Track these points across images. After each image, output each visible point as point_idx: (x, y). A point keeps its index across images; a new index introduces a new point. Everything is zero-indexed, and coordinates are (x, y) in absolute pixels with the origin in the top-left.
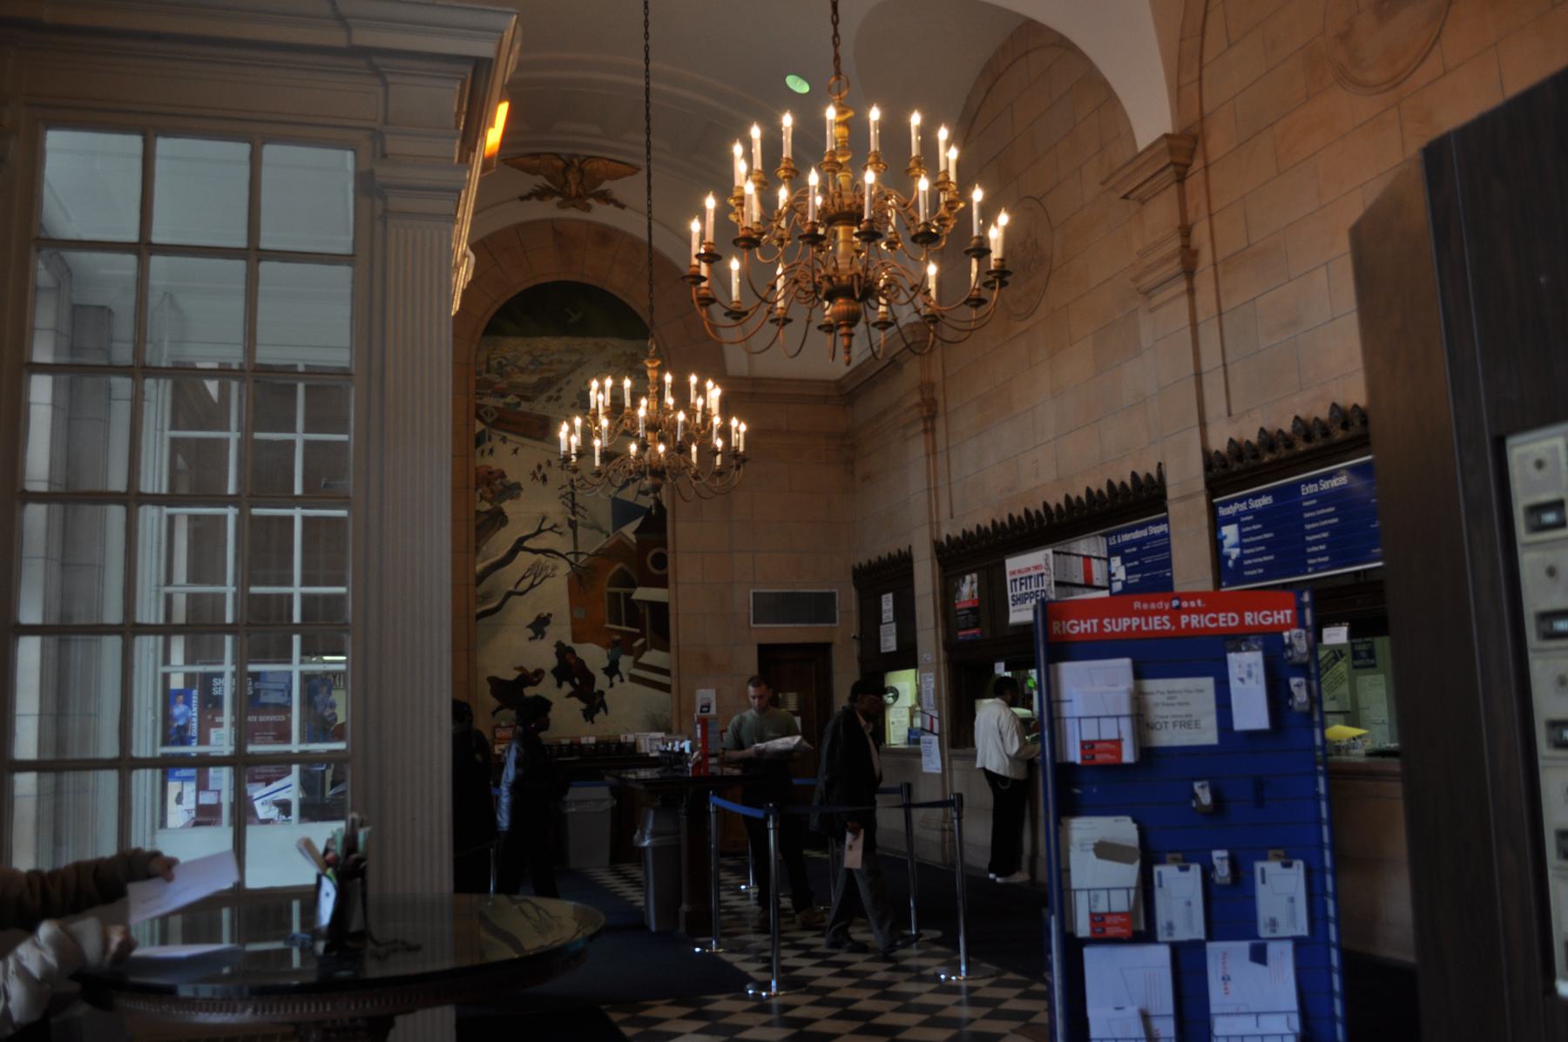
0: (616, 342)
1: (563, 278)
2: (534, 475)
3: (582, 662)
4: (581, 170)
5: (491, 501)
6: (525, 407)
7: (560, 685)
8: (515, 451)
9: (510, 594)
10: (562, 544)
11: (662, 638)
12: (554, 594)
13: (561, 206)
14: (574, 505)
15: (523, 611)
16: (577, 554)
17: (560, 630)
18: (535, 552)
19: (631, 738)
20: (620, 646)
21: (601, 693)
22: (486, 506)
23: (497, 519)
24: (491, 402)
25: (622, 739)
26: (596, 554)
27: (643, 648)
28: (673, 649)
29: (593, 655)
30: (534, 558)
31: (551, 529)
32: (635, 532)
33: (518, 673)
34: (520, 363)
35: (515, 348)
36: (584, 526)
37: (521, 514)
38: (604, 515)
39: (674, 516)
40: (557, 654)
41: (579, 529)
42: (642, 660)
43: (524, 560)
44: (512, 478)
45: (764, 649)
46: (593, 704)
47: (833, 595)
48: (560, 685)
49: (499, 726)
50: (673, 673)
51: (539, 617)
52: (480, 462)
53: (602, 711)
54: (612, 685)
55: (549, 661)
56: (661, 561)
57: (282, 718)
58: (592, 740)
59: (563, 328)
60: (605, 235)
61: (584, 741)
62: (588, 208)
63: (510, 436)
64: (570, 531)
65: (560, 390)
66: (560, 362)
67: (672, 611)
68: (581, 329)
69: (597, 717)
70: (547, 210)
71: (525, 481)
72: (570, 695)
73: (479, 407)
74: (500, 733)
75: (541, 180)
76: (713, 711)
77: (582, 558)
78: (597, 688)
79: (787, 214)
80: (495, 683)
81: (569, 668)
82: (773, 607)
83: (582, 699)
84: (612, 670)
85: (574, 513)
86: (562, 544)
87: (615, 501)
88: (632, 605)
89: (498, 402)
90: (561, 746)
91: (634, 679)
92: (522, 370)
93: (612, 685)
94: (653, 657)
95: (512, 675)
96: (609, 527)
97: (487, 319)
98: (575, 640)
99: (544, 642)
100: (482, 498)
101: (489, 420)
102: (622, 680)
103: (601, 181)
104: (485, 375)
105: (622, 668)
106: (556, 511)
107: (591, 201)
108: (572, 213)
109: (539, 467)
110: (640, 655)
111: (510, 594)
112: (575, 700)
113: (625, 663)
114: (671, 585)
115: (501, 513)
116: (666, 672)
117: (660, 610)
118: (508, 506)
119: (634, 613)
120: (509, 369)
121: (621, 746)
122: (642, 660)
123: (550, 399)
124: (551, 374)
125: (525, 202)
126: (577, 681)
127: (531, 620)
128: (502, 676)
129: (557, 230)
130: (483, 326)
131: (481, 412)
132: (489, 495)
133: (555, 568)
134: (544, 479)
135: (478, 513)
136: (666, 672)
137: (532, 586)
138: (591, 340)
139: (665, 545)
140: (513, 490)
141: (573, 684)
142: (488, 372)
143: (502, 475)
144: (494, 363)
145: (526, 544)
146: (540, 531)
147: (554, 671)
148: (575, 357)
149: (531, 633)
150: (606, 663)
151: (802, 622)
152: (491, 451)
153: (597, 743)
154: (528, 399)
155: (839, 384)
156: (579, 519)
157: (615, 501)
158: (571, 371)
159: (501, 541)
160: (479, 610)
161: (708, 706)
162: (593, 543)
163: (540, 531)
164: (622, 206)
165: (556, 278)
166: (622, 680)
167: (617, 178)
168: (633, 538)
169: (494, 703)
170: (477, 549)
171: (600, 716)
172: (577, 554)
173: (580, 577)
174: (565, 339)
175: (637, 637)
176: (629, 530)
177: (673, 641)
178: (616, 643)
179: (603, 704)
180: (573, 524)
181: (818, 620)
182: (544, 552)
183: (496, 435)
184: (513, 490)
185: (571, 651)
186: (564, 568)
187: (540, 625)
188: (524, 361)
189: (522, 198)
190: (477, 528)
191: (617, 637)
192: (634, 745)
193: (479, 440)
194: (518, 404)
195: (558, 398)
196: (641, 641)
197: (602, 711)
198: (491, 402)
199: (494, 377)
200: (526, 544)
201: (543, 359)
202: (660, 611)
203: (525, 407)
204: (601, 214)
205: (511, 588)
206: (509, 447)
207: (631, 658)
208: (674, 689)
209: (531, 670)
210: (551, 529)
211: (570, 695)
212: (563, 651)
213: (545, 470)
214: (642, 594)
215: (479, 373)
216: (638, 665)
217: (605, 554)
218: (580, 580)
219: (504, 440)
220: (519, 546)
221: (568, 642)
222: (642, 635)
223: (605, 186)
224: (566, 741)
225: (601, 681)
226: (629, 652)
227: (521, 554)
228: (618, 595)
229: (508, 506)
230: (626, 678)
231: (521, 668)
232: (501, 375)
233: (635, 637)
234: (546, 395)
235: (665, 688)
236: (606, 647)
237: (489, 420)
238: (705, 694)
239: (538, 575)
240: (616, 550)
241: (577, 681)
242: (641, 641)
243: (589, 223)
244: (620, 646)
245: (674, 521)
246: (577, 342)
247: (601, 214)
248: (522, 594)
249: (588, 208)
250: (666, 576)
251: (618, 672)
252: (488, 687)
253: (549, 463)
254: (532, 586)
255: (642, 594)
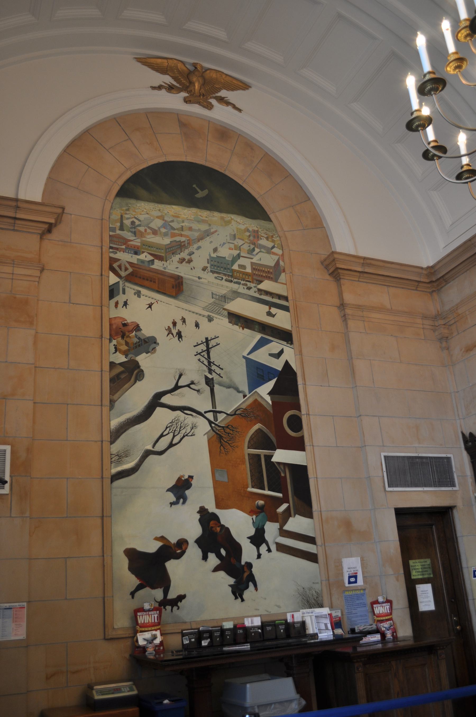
2: (170, 332)
3: (227, 530)
4: (203, 77)
5: (126, 354)
6: (158, 265)
7: (205, 558)
8: (150, 306)
9: (147, 453)
10: (203, 403)
11: (304, 506)
12: (194, 456)
13: (186, 101)
14: (209, 363)
15: (162, 473)
16: (215, 413)
17: (203, 495)
18: (173, 408)
19: (298, 617)
21: (249, 565)
22: (121, 358)
23: (130, 373)
24: (125, 257)
25: (289, 620)
26: (234, 414)
27: (287, 514)
28: (315, 514)
29: (239, 523)
31: (188, 386)
32: (269, 394)
33: (159, 544)
34: (152, 225)
35: (148, 212)
36: (220, 384)
37: (157, 370)
38: (241, 377)
39: (304, 379)
40: (201, 521)
42: (287, 527)
43: (161, 417)
44: (147, 332)
45: (400, 513)
46: (243, 580)
47: (448, 459)
48: (205, 558)
49: (142, 610)
50: (319, 541)
51: (179, 479)
52: (114, 313)
54: (259, 556)
55: (193, 530)
56: (296, 423)
58: (257, 622)
60: (224, 133)
61: (248, 623)
62: (210, 107)
63: (144, 291)
64: (208, 389)
65: (191, 254)
66: (190, 229)
68: (207, 204)
69: (247, 594)
72: (216, 569)
73: (112, 260)
74: (143, 619)
75: (168, 79)
76: (360, 581)
77: (221, 417)
78: (245, 559)
80: (133, 555)
81: (214, 538)
82: (405, 470)
83: (230, 573)
84: (258, 539)
85: (210, 371)
87: (249, 362)
88: (272, 466)
89: (134, 259)
90: (223, 631)
91: (282, 548)
92: (155, 232)
93: (259, 556)
94: (297, 524)
95: (152, 547)
96: (245, 388)
98: (218, 506)
99: (186, 506)
101: (123, 274)
102: (269, 550)
103: (219, 90)
104: (118, 232)
105: (268, 536)
106: (194, 371)
107: (213, 102)
108: (196, 109)
109: (174, 324)
110: (285, 522)
111: (147, 453)
112: (222, 574)
113: (271, 530)
114: (308, 448)
115: (137, 365)
117: (300, 473)
118: (143, 360)
120: (142, 229)
121: (289, 626)
122: (287, 527)
123: (182, 261)
124: (183, 239)
125: (156, 92)
126: (223, 552)
127: (172, 483)
128: (140, 548)
129: (184, 124)
130: (116, 188)
131: (115, 265)
132: (124, 348)
133: (194, 427)
134: (179, 335)
135: (112, 365)
137: (171, 445)
138: (216, 214)
139: (298, 407)
140: (148, 344)
141: (219, 556)
142: (122, 228)
143: (137, 328)
144: (127, 222)
145: (164, 400)
146: (177, 387)
147: (199, 541)
148: (204, 227)
149: (171, 497)
150: (252, 532)
151: (430, 486)
152: (125, 304)
153: (263, 625)
154: (160, 258)
155: (431, 270)
156: (214, 376)
158: (200, 239)
159: (136, 397)
161: (356, 577)
162: (230, 402)
163: (177, 387)
166: (269, 550)
167: (233, 90)
168: (268, 399)
169: (133, 581)
170: (112, 403)
171: (249, 593)
172: (215, 413)
173: (220, 437)
174: (194, 210)
176: (265, 390)
177: (315, 506)
178: (260, 509)
179: (252, 578)
180: (209, 382)
181: (440, 484)
182: (182, 409)
183: (131, 289)
184: (148, 344)
185: (215, 517)
186: (203, 427)
187: (181, 488)
188: (156, 224)
189: (153, 88)
190: (112, 380)
191: (261, 502)
192: (303, 624)
193: (113, 292)
194: (152, 262)
195: (190, 261)
198: (125, 257)
200: (164, 400)
201: (175, 225)
202: (300, 473)
203: (158, 265)
204: (219, 113)
205: (149, 447)
206: (144, 302)
207: (277, 525)
208: (321, 558)
209: (173, 540)
210: (188, 386)
211: (216, 569)
212: (207, 518)
213: (180, 326)
214: (281, 456)
215: (113, 230)
218: (221, 439)
219: (138, 294)
220: (156, 402)
221: (211, 508)
222: (285, 500)
223: (223, 93)
224: (228, 625)
225: (248, 553)
226: (274, 518)
227: (159, 410)
228: (258, 456)
229: (143, 360)
230: (273, 547)
231: (162, 538)
232: (135, 233)
233: (279, 502)
236: (251, 513)
237: (123, 274)
238: (351, 564)
239: (175, 436)
240: (254, 411)
241: (223, 552)
243: (209, 121)
244: (265, 512)
246: (204, 214)
247: (219, 113)
248: (161, 453)
249: (210, 107)
250: (302, 438)
252: (125, 562)
253: (184, 320)
254: (171, 445)
255: (281, 456)
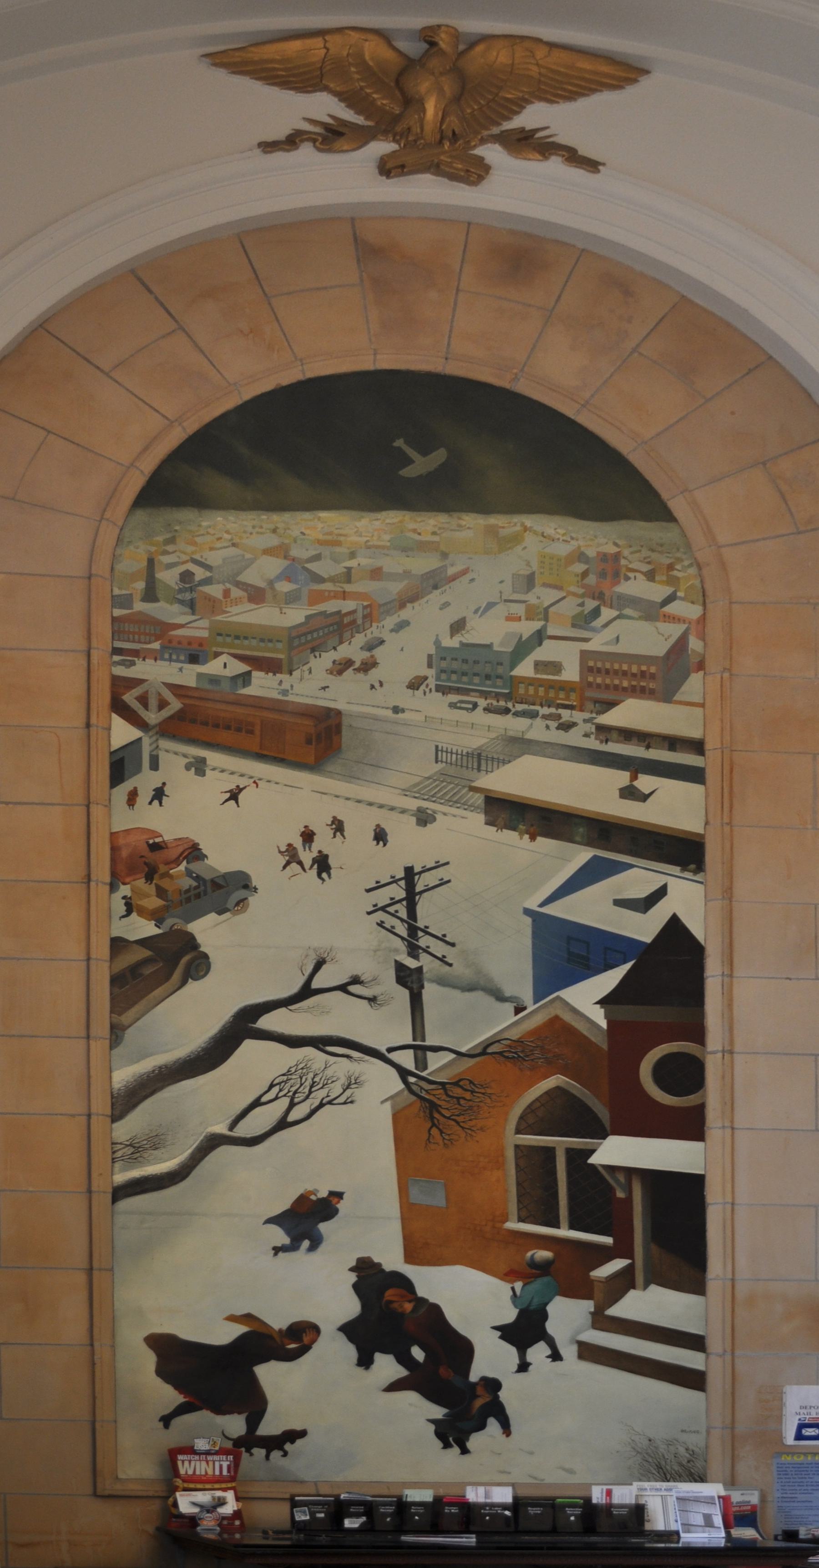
0: (552, 526)
1: (386, 362)
2: (291, 856)
3: (435, 1310)
5: (157, 917)
6: (263, 685)
7: (365, 1361)
8: (234, 796)
9: (213, 1142)
10: (388, 1027)
12: (355, 1146)
13: (388, 168)
14: (413, 931)
20: (569, 1273)
21: (493, 1385)
24: (158, 673)
25: (597, 1496)
26: (483, 1050)
27: (624, 1283)
29: (470, 1298)
30: (284, 1058)
31: (343, 988)
33: (240, 1329)
34: (251, 577)
36: (442, 982)
41: (430, 992)
42: (615, 1311)
44: (220, 860)
46: (467, 1410)
48: (365, 1361)
49: (190, 1450)
50: (714, 1344)
51: (303, 1199)
52: (123, 819)
53: (493, 1425)
54: (523, 1367)
56: (686, 1074)
57: (118, 644)
58: (503, 1495)
59: (382, 487)
61: (474, 1495)
64: (403, 994)
67: (714, 1195)
70: (349, 180)
71: (265, 870)
72: (395, 1386)
73: (120, 685)
75: (324, 106)
79: (619, 609)
81: (391, 1322)
83: (432, 1395)
84: (525, 1331)
85: (414, 950)
86: (388, 1027)
87: (542, 923)
89: (188, 675)
90: (402, 1506)
91: (589, 1353)
92: (256, 596)
93: (523, 1367)
94: (648, 1303)
96: (526, 994)
97: (149, 464)
98: (411, 1257)
100: (130, 908)
101: (153, 717)
102: (556, 1356)
103: (519, 105)
104: (139, 606)
106: (364, 948)
107: (492, 153)
108: (424, 190)
109: (308, 836)
111: (213, 1142)
112: (411, 1398)
113: (567, 1316)
115: (190, 943)
116: (696, 1343)
118: (207, 930)
119: (596, 1197)
120: (215, 591)
122: (615, 1311)
123: (342, 667)
124: (348, 605)
126: (418, 1354)
129: (373, 251)
130: (135, 483)
131: (130, 698)
132: (154, 902)
134: (322, 864)
135: (118, 945)
136: (696, 1343)
137: (283, 1124)
139: (698, 1034)
140: (227, 891)
141: (404, 1359)
142: (150, 595)
143: (194, 852)
144: (168, 577)
146: (306, 992)
147: (349, 1330)
148: (422, 564)
149: (280, 1237)
152: (159, 794)
153: (518, 1505)
154: (271, 666)
157: (542, 923)
159: (187, 1017)
160: (120, 1178)
162: (463, 1025)
163: (306, 992)
164: (592, 165)
165: (366, 364)
166: (556, 1356)
168: (599, 1016)
169: (169, 1396)
170: (116, 1033)
172: (421, 1051)
174: (393, 517)
175: (604, 1255)
176: (587, 998)
177: (715, 1266)
178: (542, 1269)
180: (409, 978)
182: (320, 1043)
183: (174, 756)
184: (227, 891)
187: (305, 1220)
189: (268, 147)
190: (116, 980)
191: (544, 1254)
192: (639, 1511)
193: (121, 767)
194: (245, 679)
195: (367, 666)
196: (617, 1265)
197: (493, 1425)
198: (158, 673)
199: (167, 611)
200: (265, 1022)
201: (320, 568)
202: (679, 1203)
203: (263, 685)
205: (221, 1128)
206: (216, 784)
207: (588, 1306)
208: (714, 1381)
210: (343, 988)
211: (395, 1386)
212: (370, 1278)
214: (616, 1151)
215: (125, 601)
216: (600, 1320)
217: (514, 1055)
219: (199, 767)
220: (243, 1026)
221: (392, 1258)
222: (623, 1249)
225: (491, 1358)
226: (578, 1288)
228: (549, 1153)
229: (207, 930)
230: (569, 1352)
231: (247, 1318)
232: (192, 605)
234: (327, 659)
235: (693, 1380)
236: (509, 1275)
237: (153, 717)
242: (617, 1265)
245: (729, 974)
246: (427, 525)
249: (475, 173)
250: (700, 1111)
251: (542, 1335)
252: (150, 1359)
253: (338, 827)
254: (283, 1124)
255: (616, 1151)
